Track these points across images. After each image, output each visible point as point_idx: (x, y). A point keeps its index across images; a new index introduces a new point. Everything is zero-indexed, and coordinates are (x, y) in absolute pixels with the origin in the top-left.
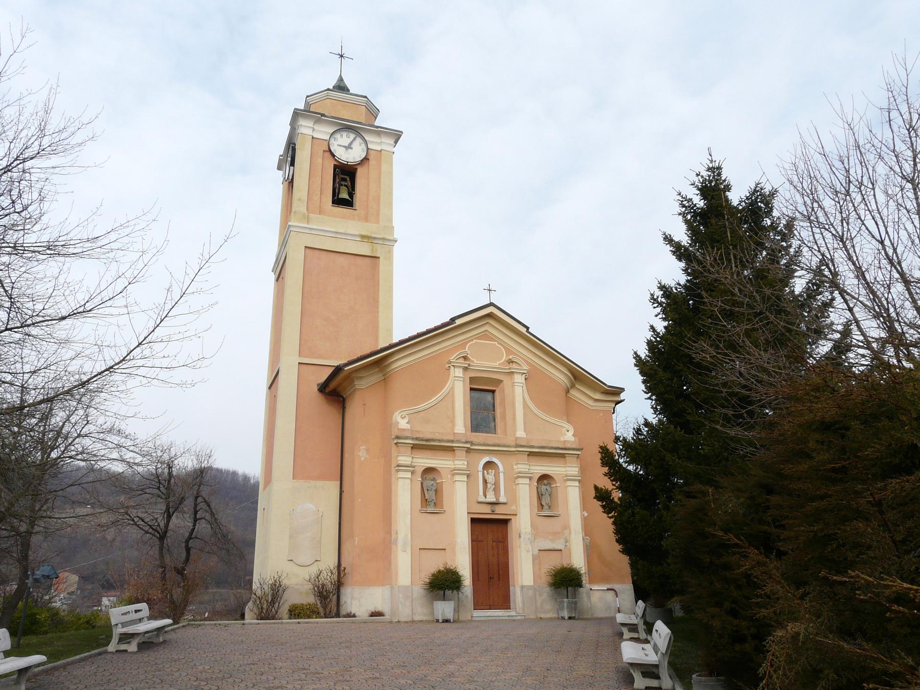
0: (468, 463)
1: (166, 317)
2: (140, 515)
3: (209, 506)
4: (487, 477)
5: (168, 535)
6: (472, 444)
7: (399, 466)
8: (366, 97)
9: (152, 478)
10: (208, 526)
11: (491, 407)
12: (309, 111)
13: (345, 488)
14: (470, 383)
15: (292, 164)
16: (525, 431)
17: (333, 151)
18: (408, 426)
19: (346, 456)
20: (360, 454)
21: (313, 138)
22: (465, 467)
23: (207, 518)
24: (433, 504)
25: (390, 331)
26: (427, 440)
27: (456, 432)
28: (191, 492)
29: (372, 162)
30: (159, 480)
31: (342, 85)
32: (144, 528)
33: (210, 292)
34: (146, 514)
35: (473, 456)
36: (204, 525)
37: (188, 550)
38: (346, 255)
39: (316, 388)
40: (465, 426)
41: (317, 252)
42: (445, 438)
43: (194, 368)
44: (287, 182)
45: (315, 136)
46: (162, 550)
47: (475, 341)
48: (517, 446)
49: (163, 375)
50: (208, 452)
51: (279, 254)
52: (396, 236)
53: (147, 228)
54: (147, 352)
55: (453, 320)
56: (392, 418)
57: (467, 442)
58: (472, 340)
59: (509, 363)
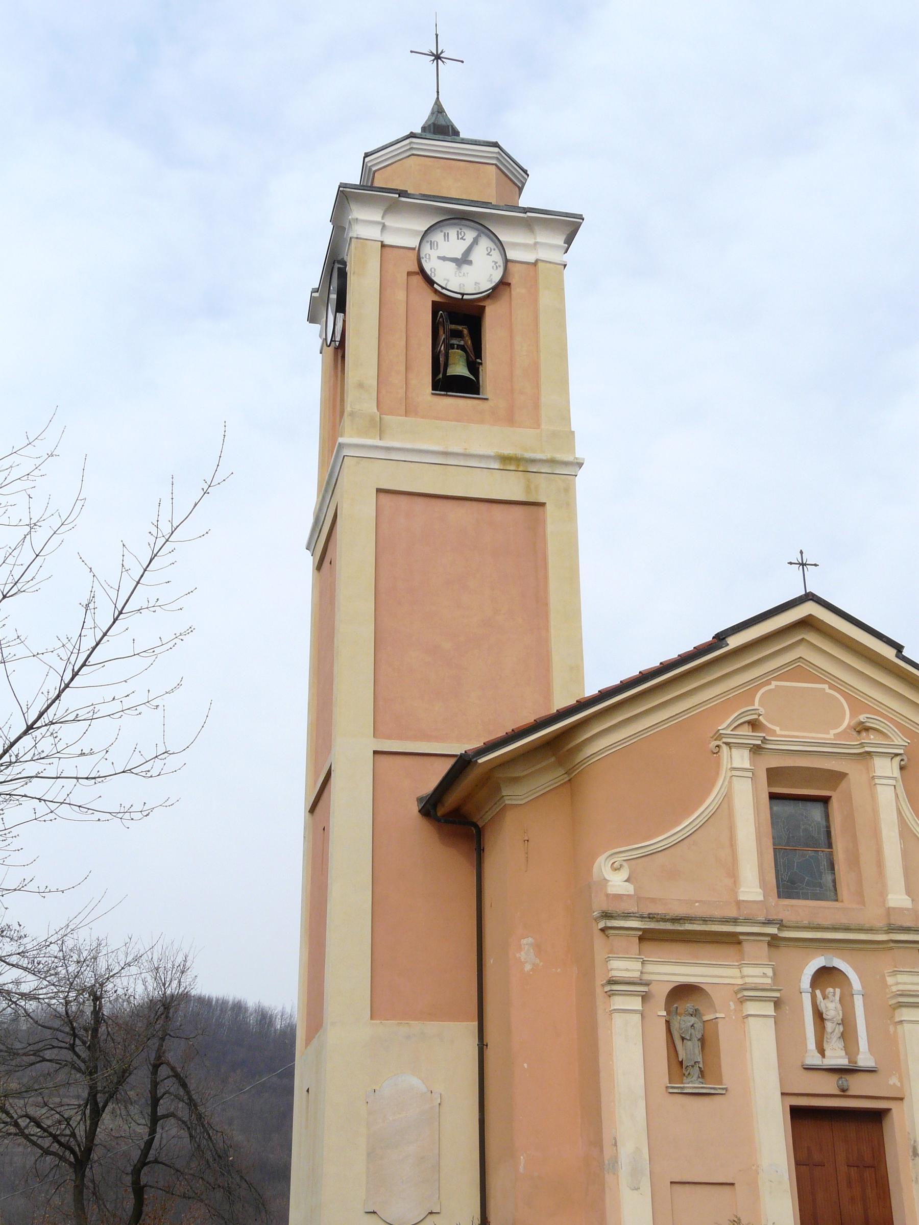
0: (774, 974)
1: (84, 665)
2: (31, 1111)
3: (184, 1085)
4: (823, 1005)
5: (94, 1156)
6: (782, 925)
7: (612, 982)
8: (495, 145)
9: (57, 1023)
10: (184, 1133)
11: (823, 838)
12: (372, 188)
13: (491, 1037)
14: (770, 782)
15: (341, 306)
16: (908, 893)
17: (429, 272)
18: (629, 889)
19: (490, 961)
20: (522, 956)
21: (383, 246)
22: (769, 981)
23: (180, 1114)
24: (696, 1072)
25: (576, 670)
26: (675, 920)
27: (742, 897)
28: (144, 1054)
29: (518, 290)
30: (73, 1029)
31: (442, 122)
32: (40, 1141)
33: (175, 606)
34: (44, 1110)
35: (787, 955)
36: (174, 1131)
37: (139, 1191)
38: (468, 503)
39: (415, 808)
40: (763, 884)
41: (403, 501)
42: (718, 913)
43: (147, 775)
44: (331, 349)
45: (387, 242)
46: (81, 1192)
47: (774, 683)
48: (891, 929)
49: (83, 793)
50: (179, 960)
51: (320, 509)
52: (580, 453)
53: (36, 472)
54: (46, 745)
55: (721, 638)
56: (590, 870)
57: (768, 922)
58: (768, 683)
59: (859, 732)
